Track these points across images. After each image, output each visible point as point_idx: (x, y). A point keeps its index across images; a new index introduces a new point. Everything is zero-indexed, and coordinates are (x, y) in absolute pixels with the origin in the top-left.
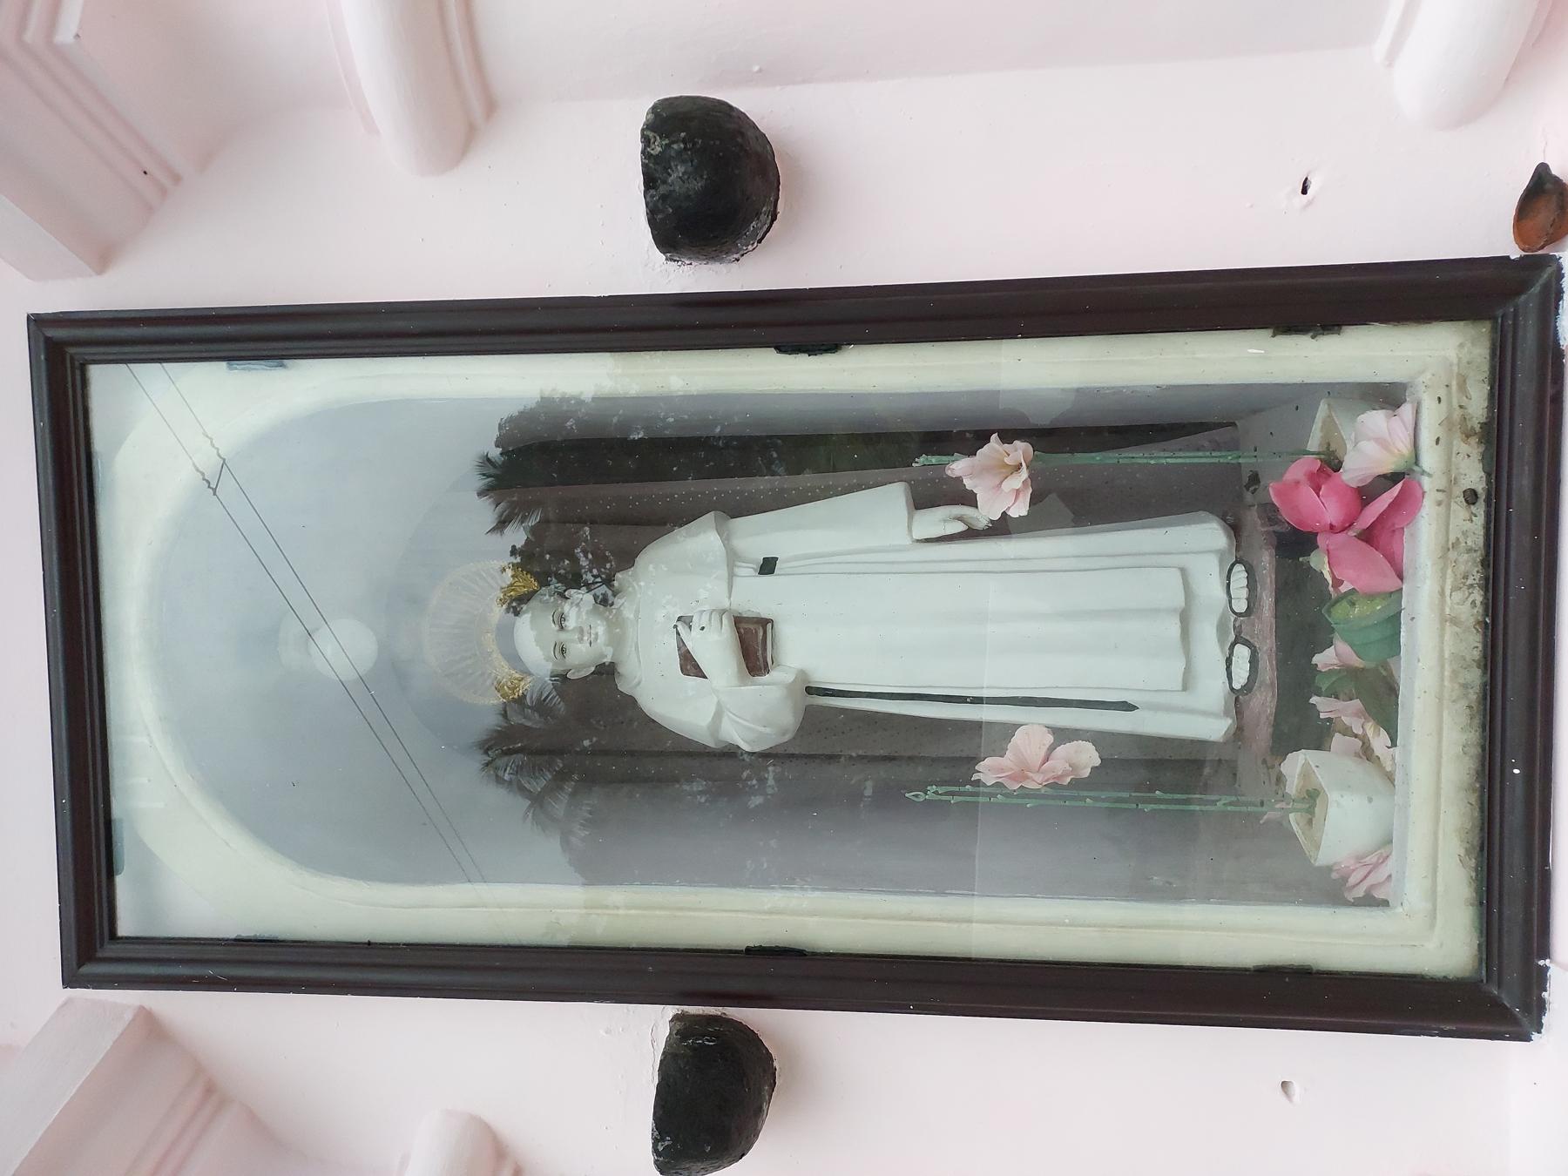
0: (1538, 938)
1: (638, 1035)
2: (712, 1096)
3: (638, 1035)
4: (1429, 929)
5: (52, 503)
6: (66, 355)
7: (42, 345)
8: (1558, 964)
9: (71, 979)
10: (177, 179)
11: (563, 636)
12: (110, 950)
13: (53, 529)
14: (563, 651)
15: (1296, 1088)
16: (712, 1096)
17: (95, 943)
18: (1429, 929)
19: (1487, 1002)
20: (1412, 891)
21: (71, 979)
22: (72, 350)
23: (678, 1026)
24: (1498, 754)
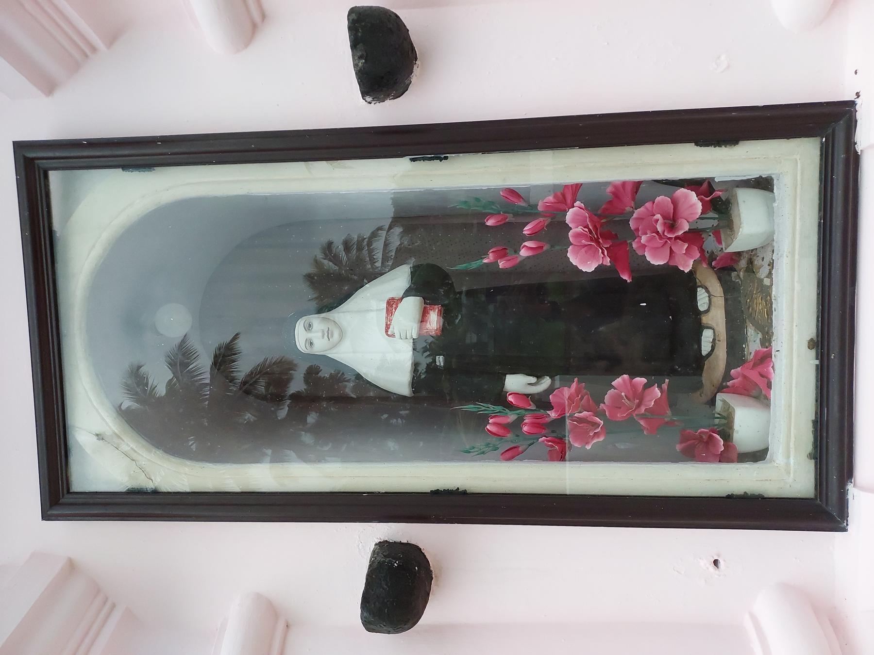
0: (847, 471)
1: (354, 545)
2: (397, 591)
3: (354, 545)
4: (789, 472)
5: (31, 267)
6: (35, 165)
7: (22, 161)
8: (862, 489)
9: (46, 517)
10: (94, 49)
11: (310, 335)
12: (67, 499)
13: (38, 356)
14: (311, 344)
15: (722, 563)
16: (397, 591)
17: (60, 496)
18: (789, 472)
19: (820, 510)
20: (778, 453)
21: (46, 517)
22: (36, 161)
23: (354, 16)
24: (826, 314)
